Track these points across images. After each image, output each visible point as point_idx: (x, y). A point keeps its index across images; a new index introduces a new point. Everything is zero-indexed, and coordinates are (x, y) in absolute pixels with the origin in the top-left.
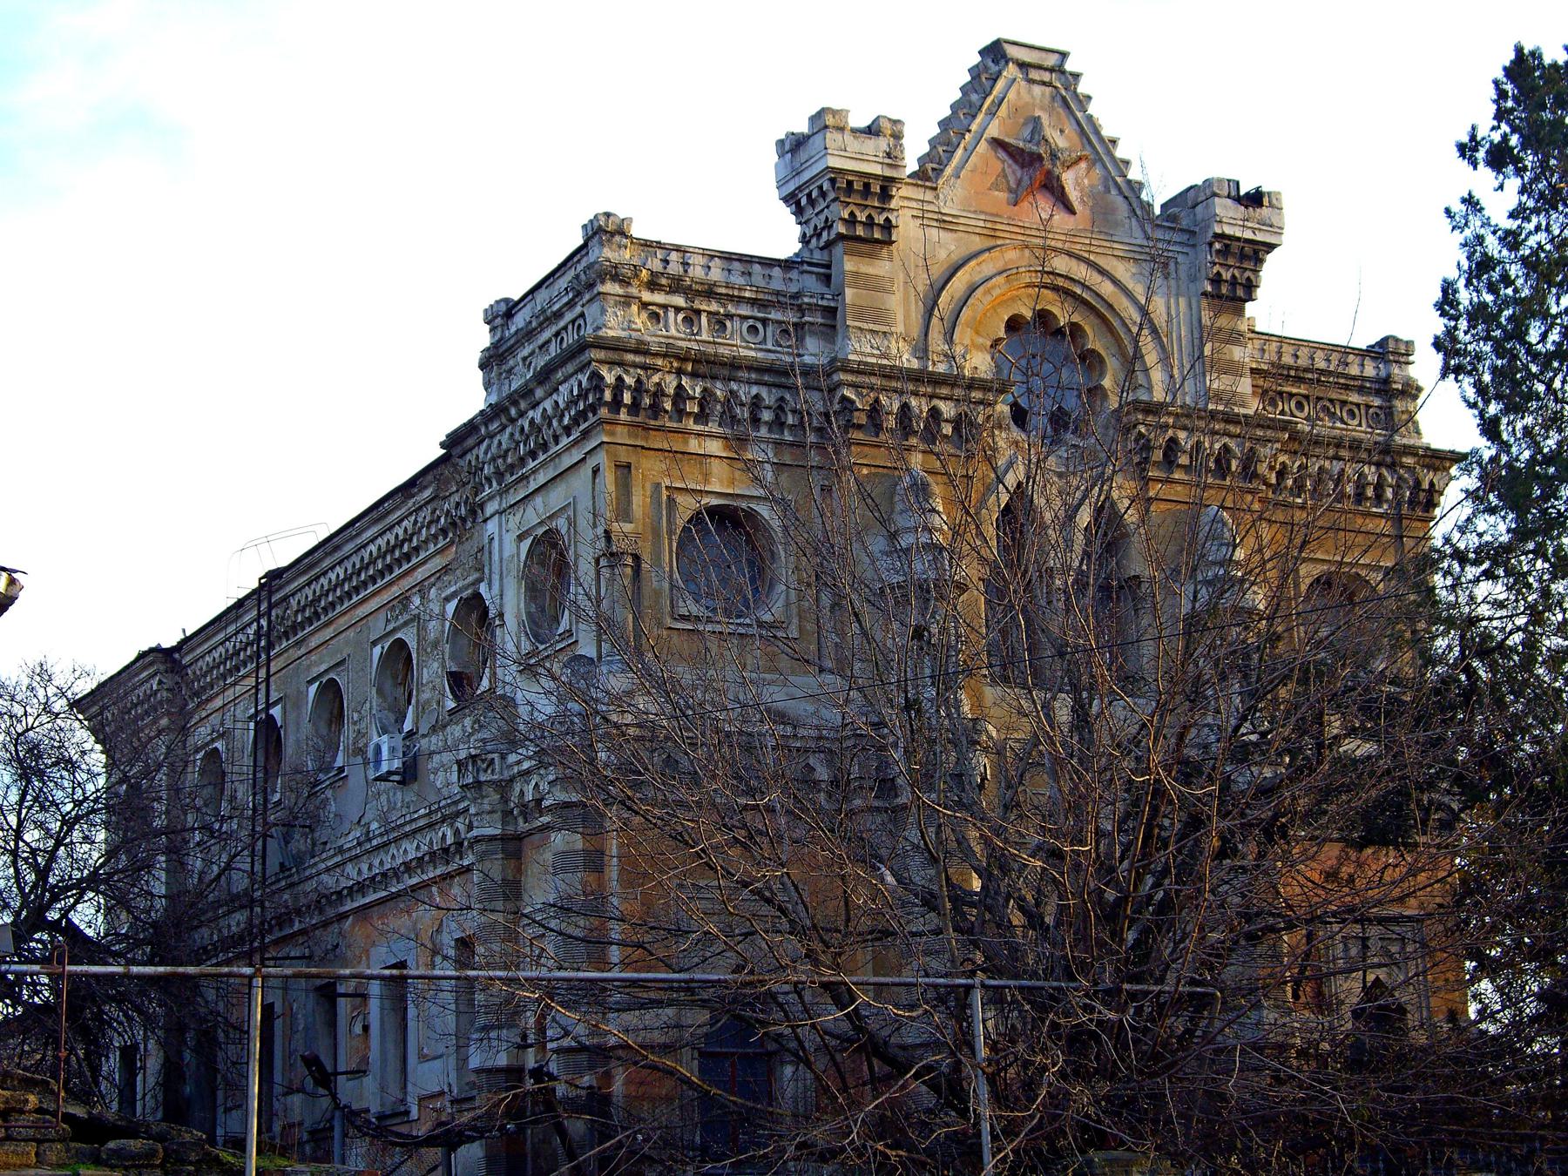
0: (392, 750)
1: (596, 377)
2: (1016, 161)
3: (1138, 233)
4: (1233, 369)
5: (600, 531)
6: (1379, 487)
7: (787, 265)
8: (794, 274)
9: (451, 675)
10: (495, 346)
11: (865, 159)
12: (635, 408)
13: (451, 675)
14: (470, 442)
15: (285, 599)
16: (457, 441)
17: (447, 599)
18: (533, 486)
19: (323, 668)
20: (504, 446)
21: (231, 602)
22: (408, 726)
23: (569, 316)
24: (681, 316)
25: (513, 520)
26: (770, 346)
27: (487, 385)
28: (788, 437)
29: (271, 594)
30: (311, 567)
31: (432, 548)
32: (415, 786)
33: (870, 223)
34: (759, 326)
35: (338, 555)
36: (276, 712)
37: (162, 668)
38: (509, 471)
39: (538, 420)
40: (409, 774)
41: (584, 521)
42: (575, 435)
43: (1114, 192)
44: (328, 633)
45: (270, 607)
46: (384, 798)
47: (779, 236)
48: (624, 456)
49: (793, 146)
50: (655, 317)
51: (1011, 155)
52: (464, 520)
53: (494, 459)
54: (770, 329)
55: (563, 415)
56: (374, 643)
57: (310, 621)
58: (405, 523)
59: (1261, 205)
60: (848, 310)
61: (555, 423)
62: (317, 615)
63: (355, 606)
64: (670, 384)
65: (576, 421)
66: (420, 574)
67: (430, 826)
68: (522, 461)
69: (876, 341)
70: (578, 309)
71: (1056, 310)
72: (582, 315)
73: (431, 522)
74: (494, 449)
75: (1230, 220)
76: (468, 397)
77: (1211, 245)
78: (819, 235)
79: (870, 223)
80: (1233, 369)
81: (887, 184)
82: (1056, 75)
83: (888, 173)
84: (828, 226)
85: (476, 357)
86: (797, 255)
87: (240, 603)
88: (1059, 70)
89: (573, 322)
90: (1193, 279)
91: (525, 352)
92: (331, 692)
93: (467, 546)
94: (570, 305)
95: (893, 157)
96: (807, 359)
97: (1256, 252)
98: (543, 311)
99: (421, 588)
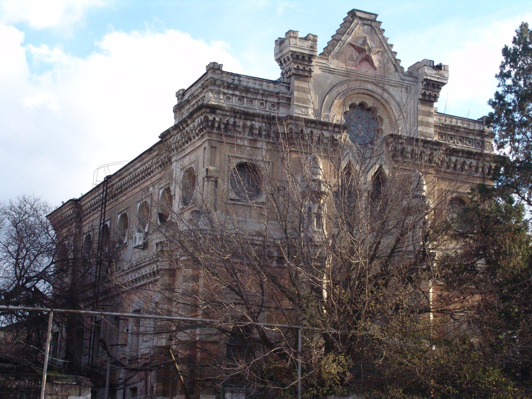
0: (140, 238)
1: (206, 118)
2: (357, 51)
3: (398, 77)
4: (428, 124)
5: (205, 168)
6: (477, 168)
7: (275, 82)
8: (277, 86)
9: (160, 214)
10: (178, 105)
11: (304, 48)
12: (219, 128)
13: (160, 214)
14: (168, 137)
15: (112, 185)
16: (164, 136)
17: (160, 189)
18: (186, 153)
19: (123, 209)
20: (178, 139)
21: (94, 186)
22: (146, 230)
23: (201, 96)
24: (237, 98)
25: (181, 163)
26: (267, 110)
27: (175, 118)
28: (271, 141)
29: (107, 183)
30: (120, 175)
31: (157, 171)
32: (147, 251)
33: (304, 70)
34: (264, 103)
35: (129, 172)
36: (108, 223)
37: (74, 206)
38: (179, 147)
39: (188, 131)
40: (145, 246)
41: (201, 165)
42: (200, 136)
43: (390, 63)
44: (125, 198)
45: (107, 189)
46: (137, 254)
47: (274, 72)
48: (214, 144)
49: (280, 42)
50: (228, 98)
51: (355, 49)
52: (167, 163)
53: (175, 143)
54: (268, 104)
55: (196, 130)
56: (138, 202)
57: (120, 193)
58: (149, 162)
59: (441, 69)
60: (295, 99)
61: (194, 132)
62: (122, 192)
63: (133, 190)
64: (232, 121)
65: (200, 132)
66: (154, 179)
67: (150, 264)
68: (184, 144)
69: (303, 110)
70: (203, 94)
71: (367, 101)
72: (204, 96)
73: (157, 163)
74: (175, 139)
75: (431, 74)
76: (170, 121)
77: (423, 82)
78: (287, 73)
79: (304, 70)
80: (428, 124)
81: (311, 57)
82: (371, 22)
83: (311, 53)
84: (290, 70)
85: (172, 110)
86: (279, 79)
87: (98, 186)
88: (374, 21)
89: (202, 98)
90: (416, 93)
91: (187, 108)
92: (124, 217)
93: (168, 171)
94: (201, 92)
95: (313, 48)
96: (280, 115)
97: (438, 85)
98: (193, 94)
99: (153, 185)
